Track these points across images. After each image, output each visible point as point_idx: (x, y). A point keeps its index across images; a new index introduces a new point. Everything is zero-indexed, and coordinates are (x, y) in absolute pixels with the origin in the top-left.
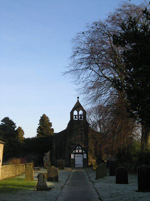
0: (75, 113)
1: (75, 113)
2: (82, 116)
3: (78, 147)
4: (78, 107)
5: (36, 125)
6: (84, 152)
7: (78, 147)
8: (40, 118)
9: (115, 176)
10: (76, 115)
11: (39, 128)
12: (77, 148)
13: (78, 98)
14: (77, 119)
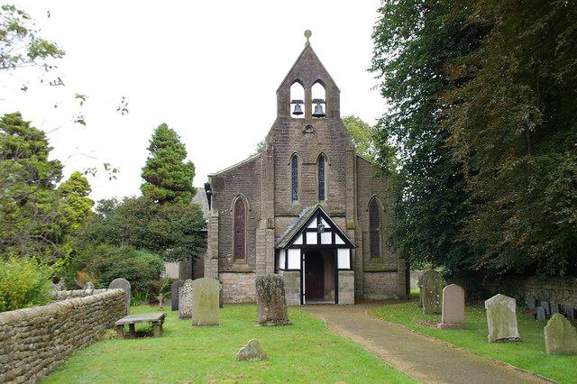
0: (297, 92)
1: (297, 92)
2: (323, 105)
3: (315, 221)
4: (308, 69)
5: (141, 156)
6: (339, 241)
7: (315, 221)
8: (182, 141)
9: (218, 184)
10: (301, 102)
11: (152, 166)
12: (314, 225)
13: (308, 34)
14: (302, 116)
